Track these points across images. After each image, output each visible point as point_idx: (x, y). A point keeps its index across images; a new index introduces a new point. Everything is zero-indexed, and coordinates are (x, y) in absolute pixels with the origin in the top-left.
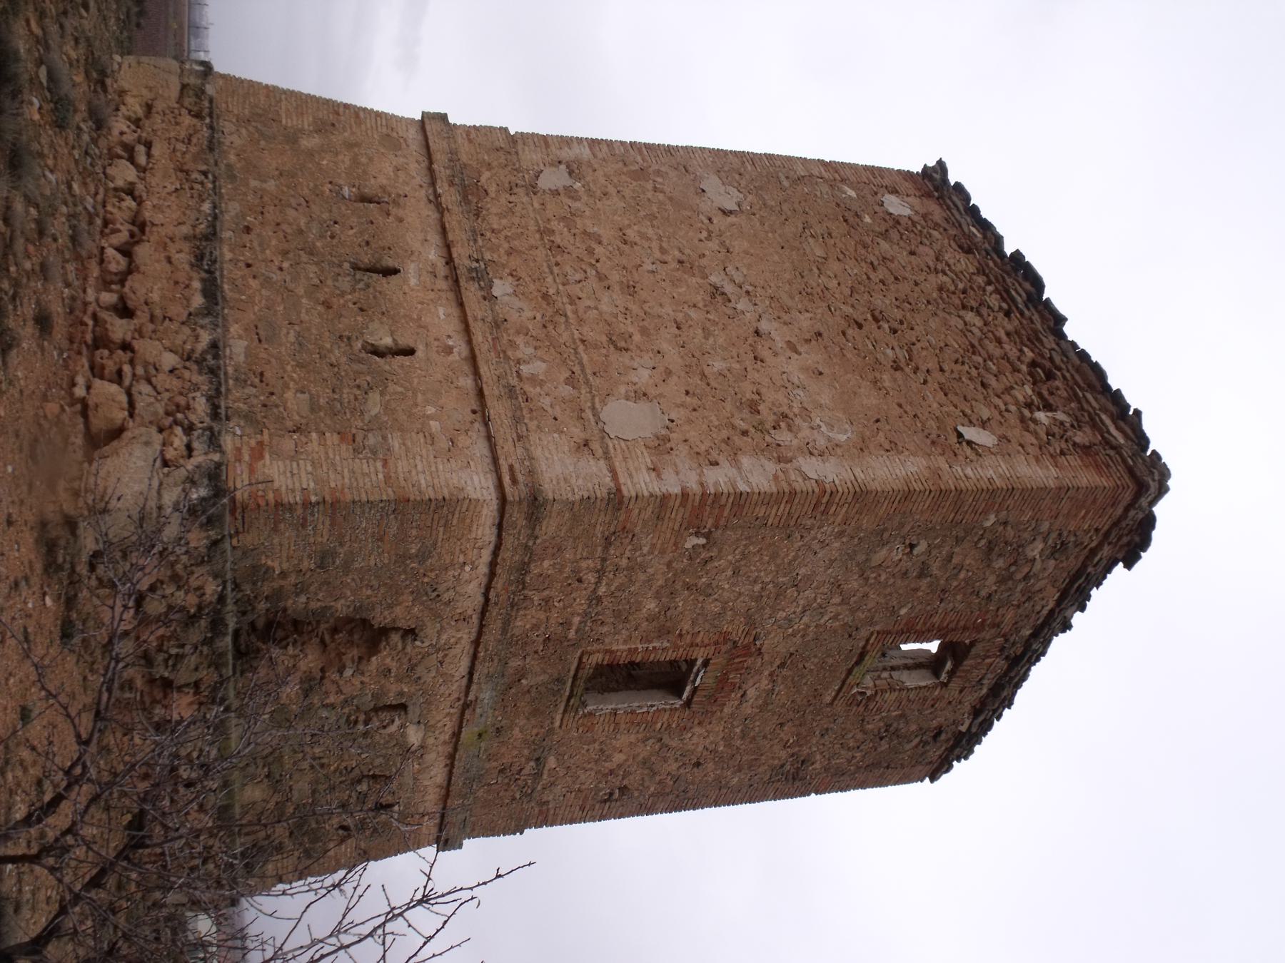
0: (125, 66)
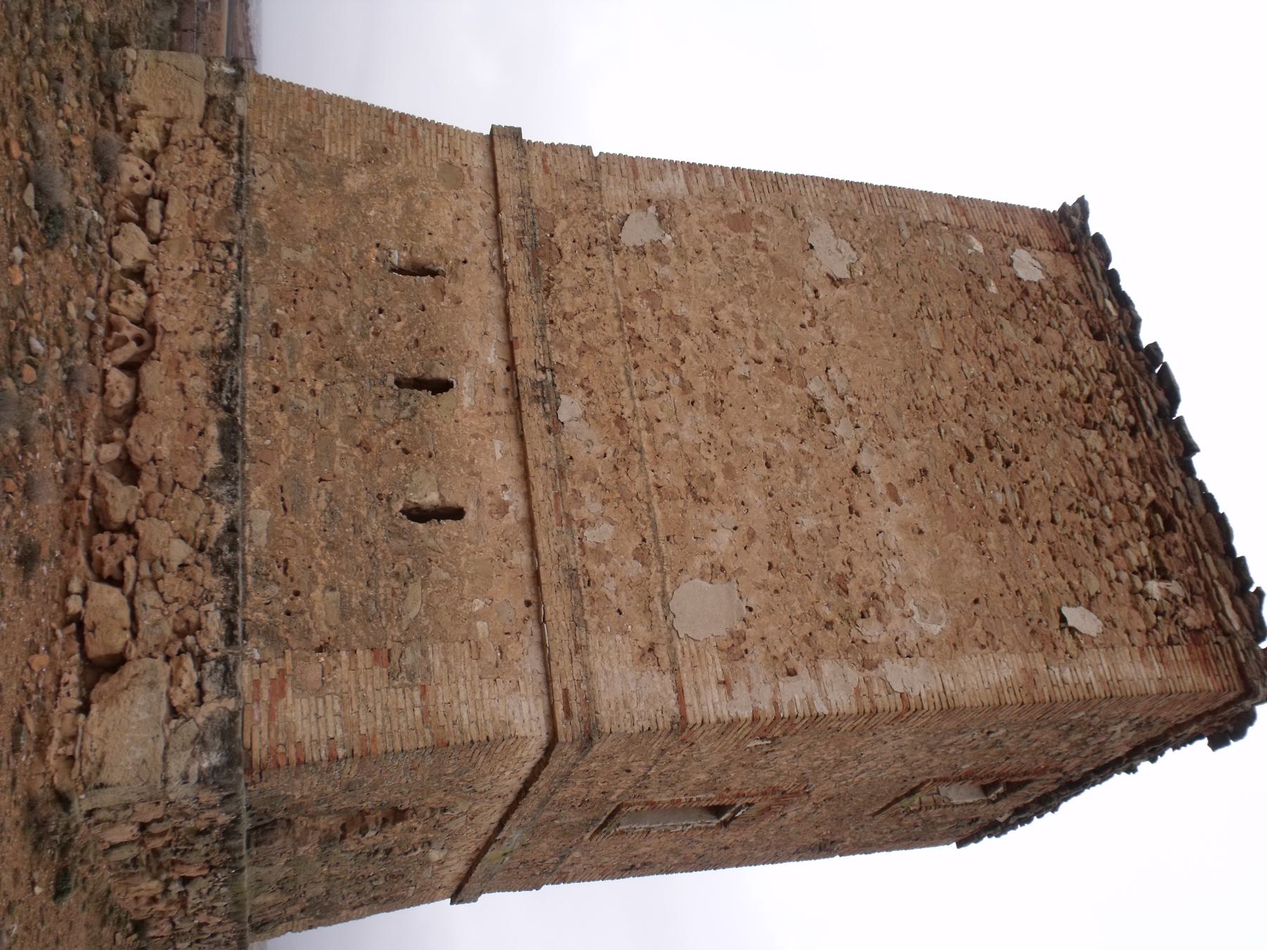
0: (140, 66)
